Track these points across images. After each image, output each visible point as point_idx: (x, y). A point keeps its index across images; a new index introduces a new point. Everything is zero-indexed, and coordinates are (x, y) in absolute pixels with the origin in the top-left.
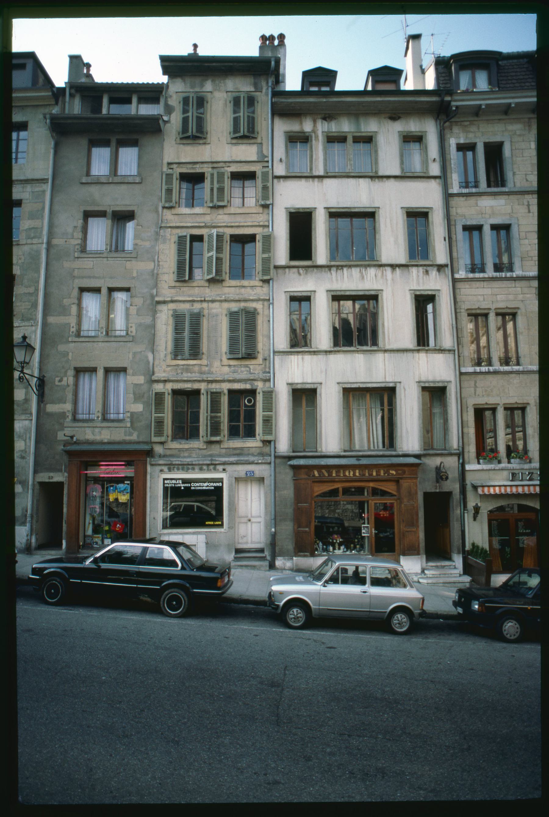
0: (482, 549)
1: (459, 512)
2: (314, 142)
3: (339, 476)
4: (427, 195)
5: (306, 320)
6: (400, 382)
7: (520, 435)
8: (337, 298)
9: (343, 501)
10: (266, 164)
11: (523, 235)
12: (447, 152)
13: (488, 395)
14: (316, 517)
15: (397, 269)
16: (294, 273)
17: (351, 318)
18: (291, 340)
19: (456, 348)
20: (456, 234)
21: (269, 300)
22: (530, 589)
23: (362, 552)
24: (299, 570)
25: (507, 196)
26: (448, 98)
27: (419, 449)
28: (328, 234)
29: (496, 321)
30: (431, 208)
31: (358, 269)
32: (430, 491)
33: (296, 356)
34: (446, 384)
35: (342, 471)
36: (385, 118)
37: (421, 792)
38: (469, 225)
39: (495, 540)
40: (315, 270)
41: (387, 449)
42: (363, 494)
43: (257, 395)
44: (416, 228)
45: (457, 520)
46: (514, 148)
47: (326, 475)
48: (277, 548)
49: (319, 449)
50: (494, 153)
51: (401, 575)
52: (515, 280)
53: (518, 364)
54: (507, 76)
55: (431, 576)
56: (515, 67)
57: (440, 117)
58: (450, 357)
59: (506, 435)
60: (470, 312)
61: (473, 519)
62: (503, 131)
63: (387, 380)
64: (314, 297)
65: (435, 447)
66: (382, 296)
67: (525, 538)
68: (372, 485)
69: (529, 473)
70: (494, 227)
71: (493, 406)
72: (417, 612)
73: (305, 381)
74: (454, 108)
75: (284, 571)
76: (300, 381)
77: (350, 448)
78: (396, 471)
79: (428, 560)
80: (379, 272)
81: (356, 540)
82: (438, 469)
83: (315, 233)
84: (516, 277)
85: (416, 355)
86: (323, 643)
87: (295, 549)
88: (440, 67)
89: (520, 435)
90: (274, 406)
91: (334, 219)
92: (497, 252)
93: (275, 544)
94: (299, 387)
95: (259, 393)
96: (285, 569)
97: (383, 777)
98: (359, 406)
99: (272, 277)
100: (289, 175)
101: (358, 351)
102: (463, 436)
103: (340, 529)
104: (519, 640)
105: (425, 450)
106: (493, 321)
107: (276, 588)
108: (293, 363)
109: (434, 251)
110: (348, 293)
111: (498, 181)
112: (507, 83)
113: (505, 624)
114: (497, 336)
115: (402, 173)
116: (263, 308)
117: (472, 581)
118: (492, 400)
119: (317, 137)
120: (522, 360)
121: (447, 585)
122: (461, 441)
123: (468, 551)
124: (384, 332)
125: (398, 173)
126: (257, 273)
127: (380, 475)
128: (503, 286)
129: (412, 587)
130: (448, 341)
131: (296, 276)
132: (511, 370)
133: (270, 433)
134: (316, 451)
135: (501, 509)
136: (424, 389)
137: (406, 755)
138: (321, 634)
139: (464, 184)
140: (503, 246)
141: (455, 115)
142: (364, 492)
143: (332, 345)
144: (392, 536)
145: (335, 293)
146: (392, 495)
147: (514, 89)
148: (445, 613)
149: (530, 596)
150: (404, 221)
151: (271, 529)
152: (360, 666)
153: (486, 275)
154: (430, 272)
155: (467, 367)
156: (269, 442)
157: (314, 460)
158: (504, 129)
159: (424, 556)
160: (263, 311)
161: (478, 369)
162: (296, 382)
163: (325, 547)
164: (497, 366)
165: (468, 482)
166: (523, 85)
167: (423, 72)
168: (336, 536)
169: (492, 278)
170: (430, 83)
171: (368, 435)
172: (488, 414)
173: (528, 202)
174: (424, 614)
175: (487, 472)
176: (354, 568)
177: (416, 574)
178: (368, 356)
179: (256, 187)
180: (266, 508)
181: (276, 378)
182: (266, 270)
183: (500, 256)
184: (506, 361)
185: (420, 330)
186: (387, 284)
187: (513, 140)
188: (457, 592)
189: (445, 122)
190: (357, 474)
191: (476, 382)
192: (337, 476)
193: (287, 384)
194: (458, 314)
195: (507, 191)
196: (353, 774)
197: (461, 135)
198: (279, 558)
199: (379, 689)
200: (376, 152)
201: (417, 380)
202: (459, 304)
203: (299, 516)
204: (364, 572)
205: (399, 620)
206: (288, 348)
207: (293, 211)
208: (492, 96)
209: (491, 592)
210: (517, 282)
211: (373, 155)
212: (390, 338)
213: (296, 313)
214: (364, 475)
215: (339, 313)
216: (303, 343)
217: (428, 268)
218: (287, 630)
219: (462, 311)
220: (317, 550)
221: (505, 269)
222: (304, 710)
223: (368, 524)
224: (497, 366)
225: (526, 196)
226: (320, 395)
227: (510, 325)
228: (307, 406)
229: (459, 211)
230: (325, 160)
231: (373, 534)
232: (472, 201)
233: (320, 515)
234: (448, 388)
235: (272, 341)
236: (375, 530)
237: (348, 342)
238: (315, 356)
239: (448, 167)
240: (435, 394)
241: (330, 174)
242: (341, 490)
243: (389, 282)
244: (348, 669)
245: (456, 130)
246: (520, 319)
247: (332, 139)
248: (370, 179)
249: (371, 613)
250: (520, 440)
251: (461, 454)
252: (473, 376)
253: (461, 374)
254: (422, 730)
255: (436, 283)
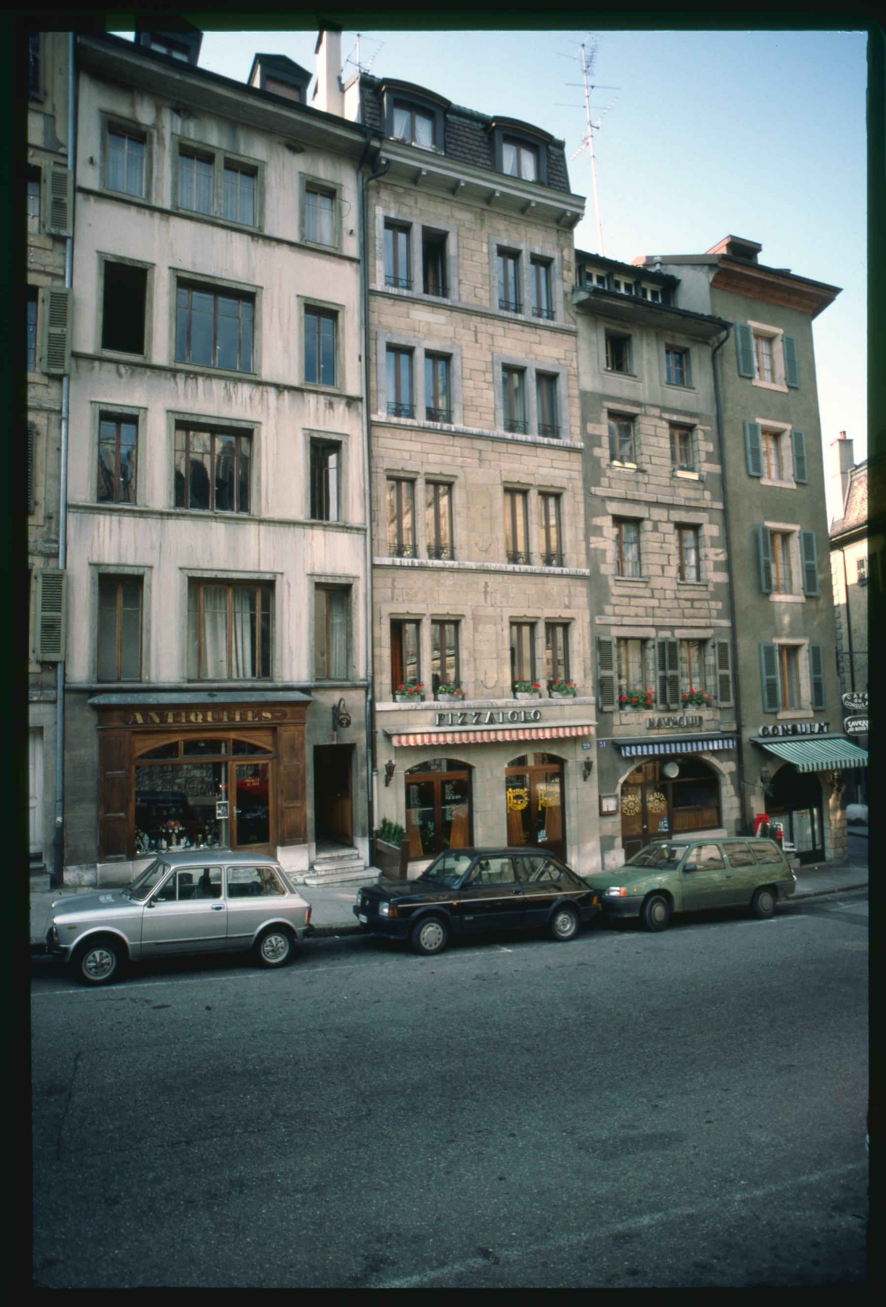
0: (397, 827)
1: (364, 774)
2: (155, 146)
3: (179, 722)
4: (338, 285)
5: (129, 455)
6: (282, 574)
7: (450, 660)
8: (185, 425)
9: (187, 764)
10: (61, 160)
11: (467, 372)
12: (370, 226)
13: (410, 601)
14: (138, 794)
15: (286, 392)
16: (109, 371)
17: (207, 462)
18: (99, 488)
19: (368, 526)
20: (376, 354)
21: (60, 412)
22: (457, 877)
23: (216, 846)
24: (106, 885)
25: (449, 312)
26: (375, 144)
27: (309, 679)
28: (174, 315)
29: (427, 491)
30: (343, 306)
31: (222, 383)
32: (324, 744)
33: (108, 517)
34: (351, 581)
35: (184, 714)
36: (279, 143)
37: (299, 1196)
38: (395, 344)
39: (415, 812)
40: (148, 372)
41: (259, 677)
42: (220, 752)
43: (33, 580)
44: (319, 333)
45: (362, 788)
46: (461, 245)
47: (157, 720)
48: (66, 851)
49: (145, 678)
50: (435, 246)
51: (279, 879)
52: (453, 436)
53: (452, 558)
54: (457, 140)
55: (323, 873)
56: (467, 130)
57: (363, 169)
58: (358, 539)
59: (434, 660)
60: (390, 473)
61: (384, 784)
62: (448, 217)
63: (262, 569)
64: (145, 419)
65: (332, 675)
66: (259, 432)
67: (453, 807)
68: (233, 735)
69: (461, 714)
70: (431, 355)
71: (417, 617)
72: (299, 929)
73: (123, 561)
74: (384, 162)
75: (80, 890)
76: (113, 560)
77: (199, 676)
78: (271, 713)
79: (319, 849)
80: (257, 392)
81: (207, 827)
82: (336, 710)
83: (152, 307)
84: (455, 432)
85: (309, 531)
86: (148, 1001)
87: (99, 849)
88: (368, 91)
89: (450, 660)
90: (64, 601)
91: (185, 291)
92: (432, 394)
93: (63, 844)
94: (112, 570)
95: (36, 578)
96: (81, 886)
97: (241, 1192)
98: (215, 608)
99: (67, 371)
100: (106, 192)
101: (216, 518)
102: (373, 659)
103: (181, 811)
104: (443, 949)
105: (317, 680)
106: (421, 490)
107: (59, 920)
108: (101, 529)
109: (343, 374)
110: (203, 420)
111: (438, 287)
112: (455, 150)
113: (424, 929)
114: (426, 515)
115: (301, 239)
116: (48, 425)
117: (383, 874)
118: (415, 609)
119: (161, 139)
120: (457, 553)
121: (346, 884)
122: (370, 667)
123: (377, 832)
124: (259, 491)
125: (295, 238)
126: (37, 358)
127: (246, 720)
128: (438, 442)
129: (292, 892)
130: (356, 515)
131: (113, 376)
132: (442, 566)
133: (56, 648)
134: (140, 681)
135: (424, 766)
136: (319, 586)
137: (279, 1148)
138: (144, 988)
139: (392, 280)
140: (441, 386)
141: (385, 173)
142: (220, 747)
143: (173, 503)
144: (265, 816)
145: (180, 417)
146: (266, 752)
147: (464, 161)
148: (343, 926)
149: (456, 887)
150: (300, 317)
151: (55, 819)
152: (209, 1028)
153: (415, 423)
154: (335, 406)
155: (382, 556)
156: (54, 664)
157: (135, 695)
158: (449, 214)
159: (314, 844)
160: (48, 431)
161: (398, 561)
162: (107, 561)
163: (153, 842)
164: (424, 559)
165: (379, 729)
166: (476, 159)
167: (342, 89)
168: (173, 823)
169: (423, 428)
170: (351, 112)
171: (228, 656)
172: (410, 628)
173: (476, 327)
174: (310, 931)
175: (405, 714)
176: (201, 872)
177: (301, 873)
178: (232, 526)
179: (40, 197)
180: (46, 781)
181: (68, 552)
182: (55, 358)
183: (435, 398)
184: (436, 552)
185: (317, 493)
186: (268, 414)
187: (461, 234)
188: (359, 893)
189: (370, 179)
190: (210, 719)
191: (394, 580)
192: (175, 721)
193: (90, 564)
194: (374, 475)
195: (449, 304)
196: (192, 1202)
197: (392, 205)
198: (70, 868)
199: (238, 1058)
200: (262, 194)
201: (309, 572)
202: (375, 460)
203: (108, 794)
204: (219, 878)
205: (272, 946)
206: (93, 502)
207: (112, 260)
208: (436, 162)
209: (408, 887)
210: (456, 439)
211: (257, 199)
212: (270, 501)
213: (111, 441)
214: (221, 720)
215: (187, 450)
216: (122, 495)
217: (334, 399)
218: (82, 990)
219: (379, 470)
220: (139, 848)
221: (441, 418)
222: (109, 1121)
223: (226, 799)
224: (424, 559)
225: (474, 318)
226: (150, 586)
227: (444, 501)
228: (125, 604)
229: (383, 319)
230: (175, 185)
231: (235, 815)
232: (402, 307)
233: (147, 789)
234: (354, 586)
235: (62, 486)
236: (238, 808)
237: (201, 501)
238: (142, 519)
239: (371, 249)
240: (334, 594)
241: (181, 211)
242: (181, 746)
243: (272, 411)
244: (189, 1036)
245: (385, 195)
246: (457, 492)
247: (191, 153)
248: (250, 238)
249: (229, 941)
250: (451, 667)
251: (369, 687)
252: (391, 570)
253: (374, 566)
254: (304, 1104)
255: (342, 423)
